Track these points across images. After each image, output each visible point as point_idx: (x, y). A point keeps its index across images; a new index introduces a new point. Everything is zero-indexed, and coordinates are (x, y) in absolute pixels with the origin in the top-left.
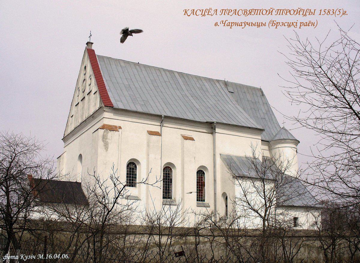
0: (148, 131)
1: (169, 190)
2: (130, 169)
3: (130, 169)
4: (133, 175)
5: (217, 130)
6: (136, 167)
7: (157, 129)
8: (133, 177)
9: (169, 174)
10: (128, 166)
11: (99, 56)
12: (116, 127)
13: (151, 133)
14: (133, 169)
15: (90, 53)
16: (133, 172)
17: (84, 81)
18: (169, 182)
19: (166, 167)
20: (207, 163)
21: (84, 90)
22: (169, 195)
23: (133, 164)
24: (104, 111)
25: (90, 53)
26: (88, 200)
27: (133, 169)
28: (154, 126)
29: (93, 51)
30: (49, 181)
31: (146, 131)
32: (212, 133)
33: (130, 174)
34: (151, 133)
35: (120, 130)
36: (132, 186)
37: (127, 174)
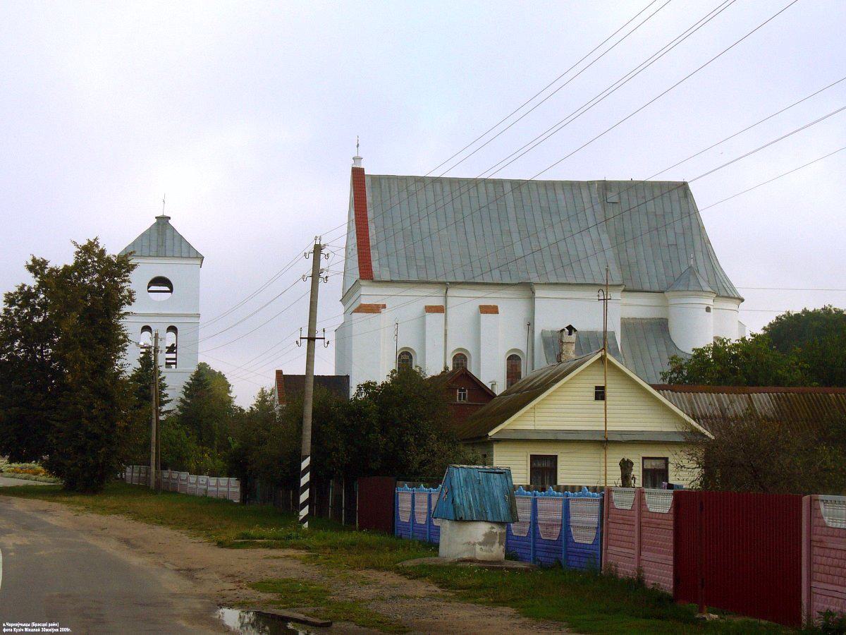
5: (539, 293)
6: (411, 357)
7: (437, 301)
11: (373, 178)
13: (430, 309)
23: (407, 353)
29: (362, 170)
34: (430, 309)
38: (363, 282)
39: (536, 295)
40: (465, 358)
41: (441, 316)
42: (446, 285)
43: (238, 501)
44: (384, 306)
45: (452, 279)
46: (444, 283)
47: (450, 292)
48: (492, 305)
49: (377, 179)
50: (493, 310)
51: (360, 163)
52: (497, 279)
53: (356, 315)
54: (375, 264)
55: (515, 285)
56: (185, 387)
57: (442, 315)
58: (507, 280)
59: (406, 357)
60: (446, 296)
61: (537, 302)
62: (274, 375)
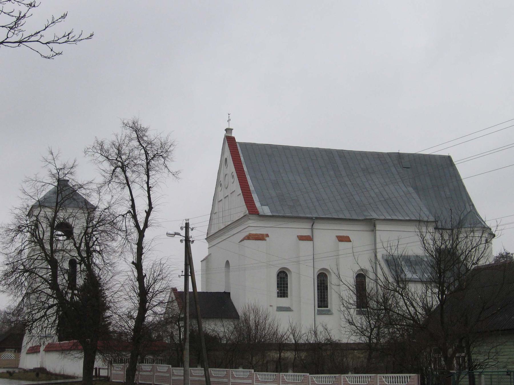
0: (298, 236)
1: (324, 298)
2: (281, 278)
3: (281, 278)
4: (284, 284)
5: (378, 227)
6: (287, 275)
7: (306, 233)
8: (284, 287)
9: (324, 280)
10: (278, 275)
11: (241, 144)
12: (262, 235)
13: (302, 238)
14: (284, 278)
15: (230, 141)
16: (284, 281)
17: (225, 176)
18: (324, 290)
19: (320, 273)
20: (367, 265)
21: (227, 186)
22: (324, 304)
23: (284, 272)
24: (249, 219)
25: (230, 141)
26: (310, 343)
27: (284, 278)
28: (304, 229)
29: (234, 139)
30: (142, 266)
31: (296, 236)
32: (373, 231)
33: (281, 284)
34: (302, 238)
35: (267, 238)
36: (284, 297)
37: (278, 284)
38: (251, 217)
39: (377, 229)
40: (326, 276)
41: (309, 243)
42: (313, 220)
43: (222, 342)
44: (267, 236)
45: (315, 215)
46: (311, 218)
47: (316, 226)
48: (345, 235)
49: (245, 145)
50: (346, 239)
51: (231, 133)
52: (348, 216)
53: (247, 242)
54: (258, 204)
55: (362, 220)
56: (74, 174)
57: (311, 242)
58: (355, 217)
59: (282, 275)
60: (312, 229)
61: (378, 233)
62: (232, 128)
